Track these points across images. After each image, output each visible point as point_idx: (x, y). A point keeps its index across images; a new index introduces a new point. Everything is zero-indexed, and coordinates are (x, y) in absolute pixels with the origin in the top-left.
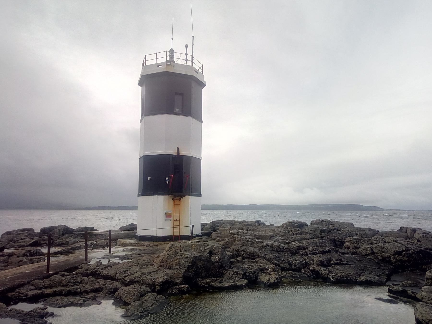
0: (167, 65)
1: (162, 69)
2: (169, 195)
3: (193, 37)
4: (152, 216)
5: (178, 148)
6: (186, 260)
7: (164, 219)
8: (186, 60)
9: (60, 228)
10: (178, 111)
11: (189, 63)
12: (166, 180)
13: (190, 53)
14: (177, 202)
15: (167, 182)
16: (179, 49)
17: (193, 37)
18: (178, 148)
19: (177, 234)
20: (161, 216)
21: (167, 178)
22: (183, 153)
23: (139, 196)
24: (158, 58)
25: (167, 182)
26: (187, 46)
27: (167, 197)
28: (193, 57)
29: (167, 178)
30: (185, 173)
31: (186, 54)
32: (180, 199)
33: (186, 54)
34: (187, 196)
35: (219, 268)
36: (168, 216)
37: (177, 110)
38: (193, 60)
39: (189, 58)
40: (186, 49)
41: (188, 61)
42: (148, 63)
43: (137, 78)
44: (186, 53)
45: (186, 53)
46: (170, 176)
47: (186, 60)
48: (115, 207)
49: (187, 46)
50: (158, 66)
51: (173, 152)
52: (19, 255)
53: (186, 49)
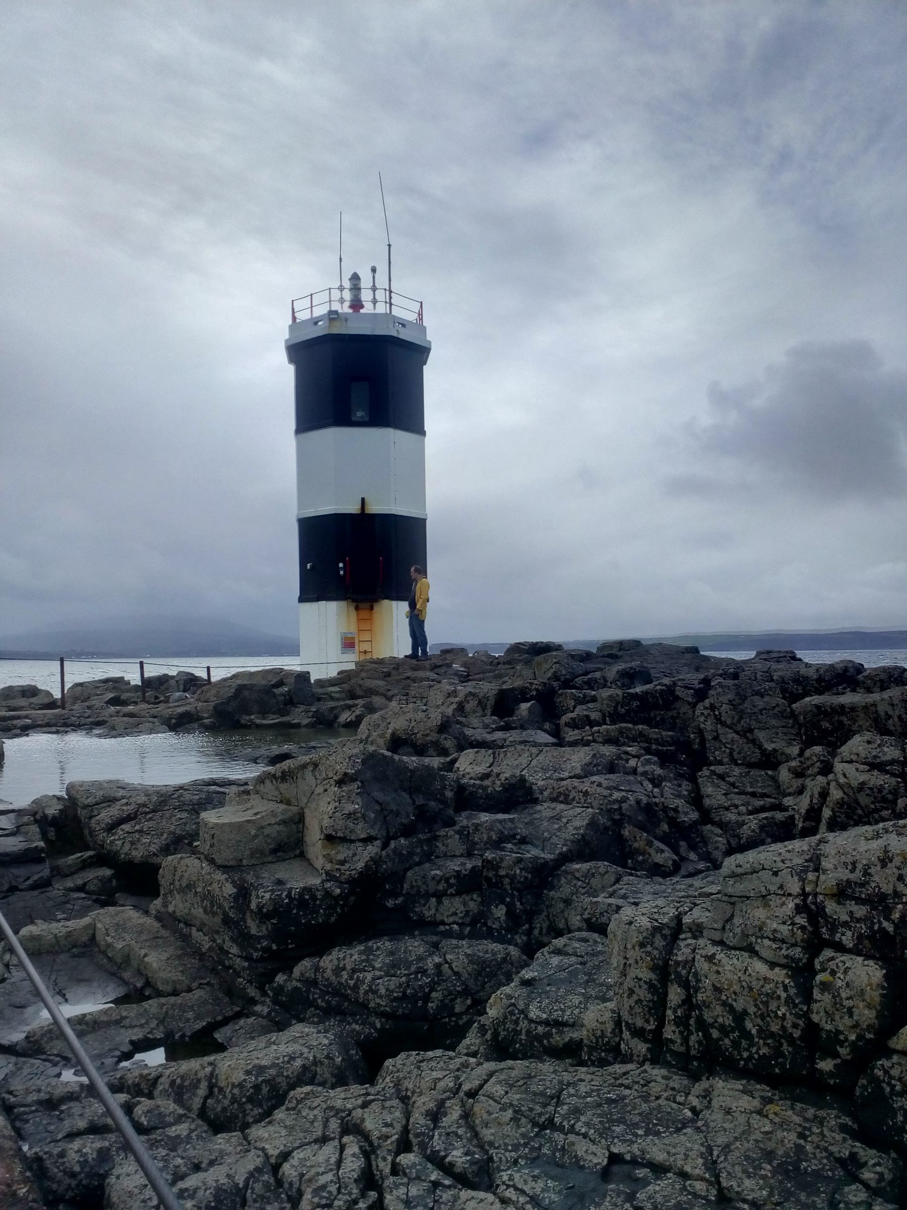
0: (331, 320)
1: (322, 329)
3: (389, 246)
4: (319, 643)
5: (363, 500)
6: (227, 689)
9: (177, 679)
10: (362, 417)
14: (364, 614)
15: (342, 573)
17: (389, 246)
18: (363, 500)
20: (335, 644)
22: (374, 508)
23: (301, 600)
25: (342, 573)
26: (374, 270)
27: (343, 604)
28: (391, 292)
29: (341, 565)
32: (372, 608)
34: (386, 602)
35: (285, 704)
37: (359, 414)
38: (390, 298)
40: (374, 277)
41: (377, 304)
44: (374, 285)
45: (374, 285)
46: (364, 556)
48: (421, 623)
49: (374, 270)
50: (316, 323)
51: (353, 508)
53: (374, 277)
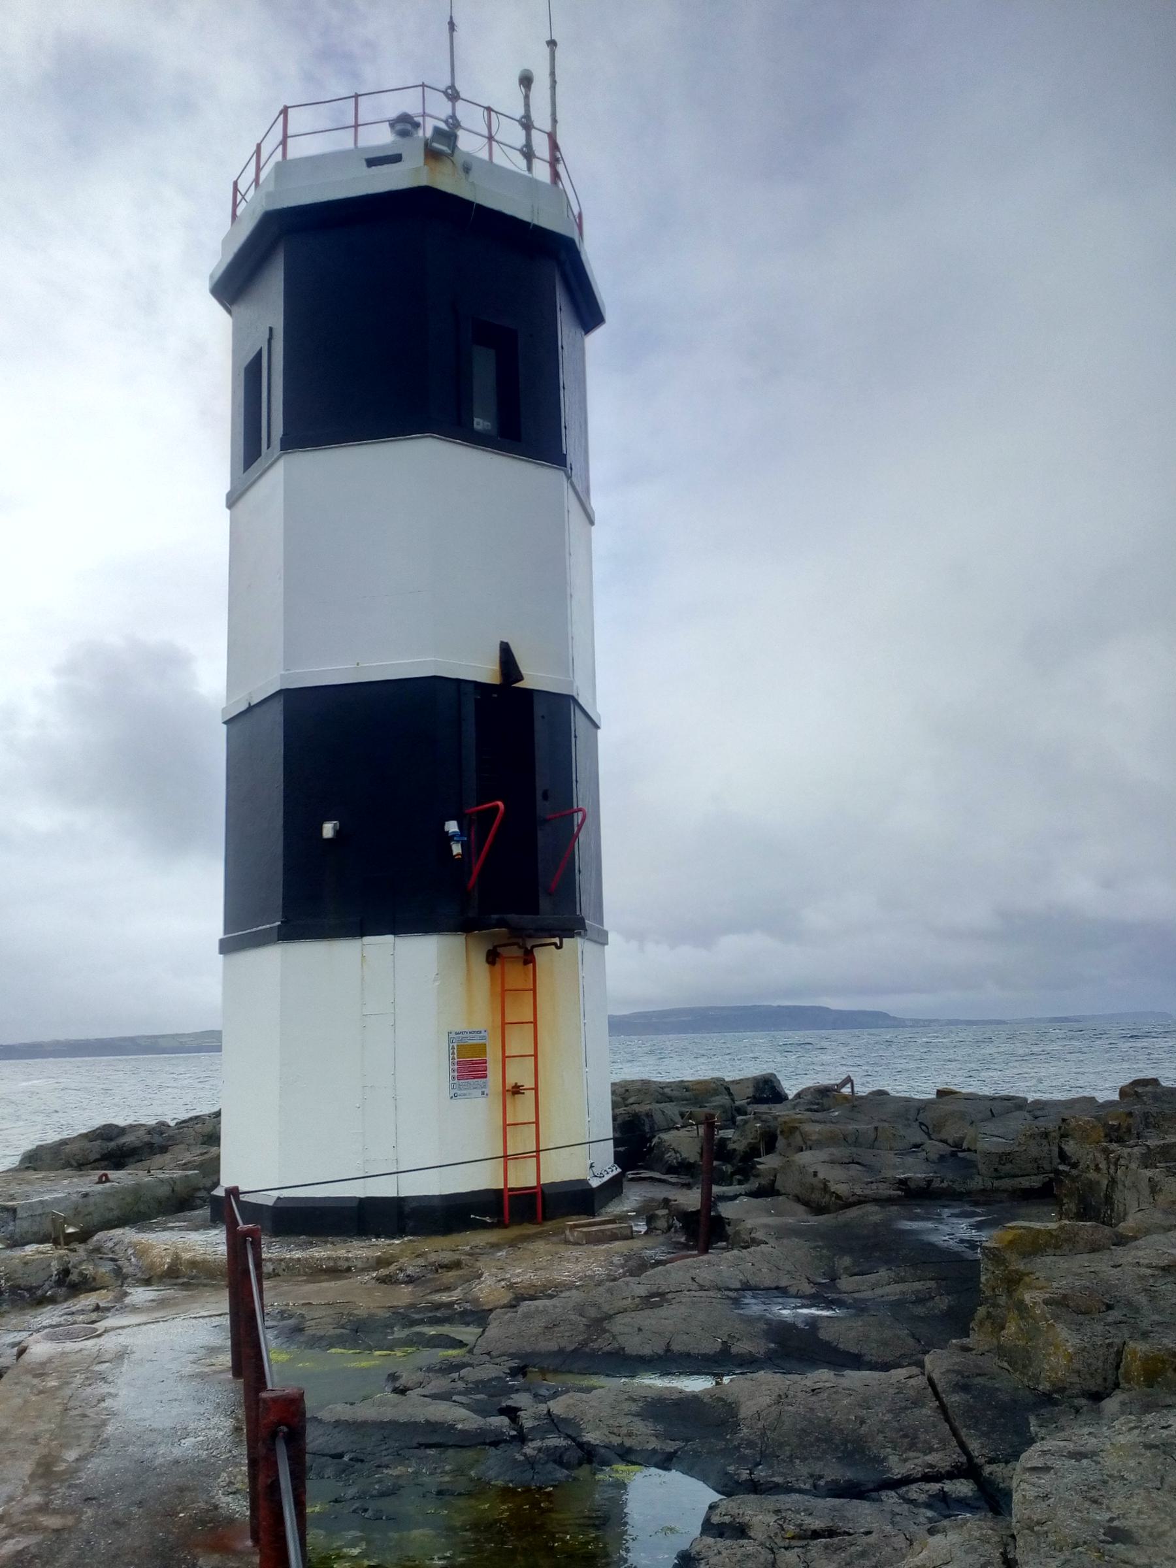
2: (464, 926)
4: (350, 1073)
7: (446, 1085)
8: (528, 154)
11: (542, 172)
12: (449, 838)
13: (541, 119)
14: (515, 975)
15: (457, 849)
16: (491, 83)
19: (523, 1177)
20: (433, 1066)
21: (452, 827)
24: (339, 151)
25: (457, 849)
26: (526, 81)
29: (452, 827)
30: (545, 796)
31: (527, 124)
33: (527, 124)
36: (469, 1066)
39: (541, 146)
40: (527, 97)
42: (299, 149)
43: (215, 240)
47: (528, 154)
49: (526, 81)
51: (482, 669)
52: (1093, 1385)
53: (527, 97)
